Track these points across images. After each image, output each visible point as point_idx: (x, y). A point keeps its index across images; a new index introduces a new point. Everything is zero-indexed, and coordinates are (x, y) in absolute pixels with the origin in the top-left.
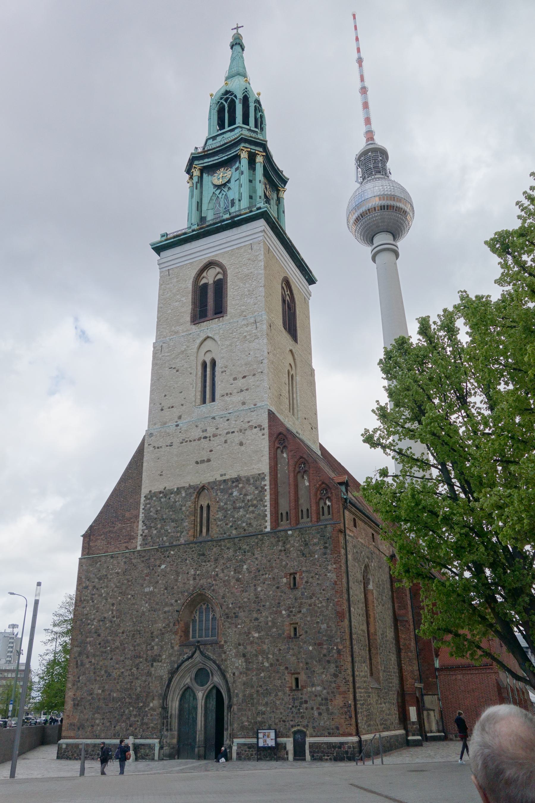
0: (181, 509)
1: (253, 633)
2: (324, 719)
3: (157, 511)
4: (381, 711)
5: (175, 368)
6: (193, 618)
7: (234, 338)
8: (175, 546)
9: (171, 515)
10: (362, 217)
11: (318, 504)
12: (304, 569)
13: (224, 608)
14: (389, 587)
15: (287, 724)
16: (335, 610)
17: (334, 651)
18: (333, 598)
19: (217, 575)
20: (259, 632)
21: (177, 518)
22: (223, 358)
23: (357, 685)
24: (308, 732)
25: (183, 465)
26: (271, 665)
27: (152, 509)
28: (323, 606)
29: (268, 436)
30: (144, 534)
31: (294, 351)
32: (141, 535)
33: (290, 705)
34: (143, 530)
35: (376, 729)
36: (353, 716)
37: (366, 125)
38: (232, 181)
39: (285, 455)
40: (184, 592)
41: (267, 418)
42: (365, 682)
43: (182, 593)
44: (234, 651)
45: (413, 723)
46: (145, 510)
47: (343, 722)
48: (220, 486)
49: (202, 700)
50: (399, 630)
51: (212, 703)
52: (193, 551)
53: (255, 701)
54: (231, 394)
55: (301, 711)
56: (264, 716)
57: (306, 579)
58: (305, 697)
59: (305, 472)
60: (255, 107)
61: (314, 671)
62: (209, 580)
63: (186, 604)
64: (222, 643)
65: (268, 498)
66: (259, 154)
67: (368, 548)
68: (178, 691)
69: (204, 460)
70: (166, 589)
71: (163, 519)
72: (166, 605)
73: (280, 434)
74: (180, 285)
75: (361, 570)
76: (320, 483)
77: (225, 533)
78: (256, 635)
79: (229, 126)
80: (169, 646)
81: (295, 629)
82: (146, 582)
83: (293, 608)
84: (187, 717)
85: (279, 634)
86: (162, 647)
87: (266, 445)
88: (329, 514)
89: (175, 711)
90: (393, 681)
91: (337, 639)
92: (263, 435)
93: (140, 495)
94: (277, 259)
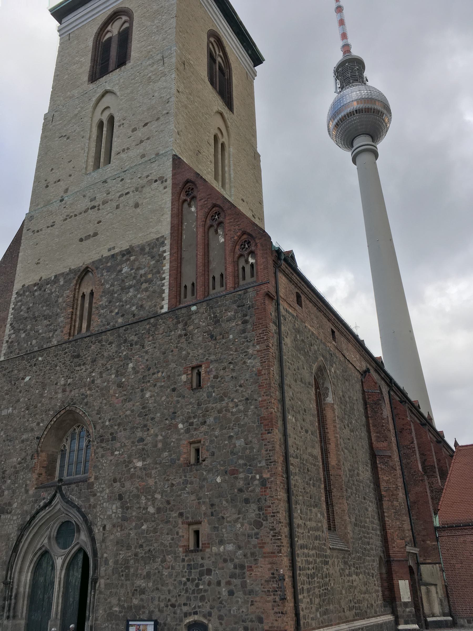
0: (57, 301)
1: (135, 461)
2: (237, 602)
3: (28, 308)
4: (351, 587)
5: (66, 136)
6: (62, 448)
7: (136, 83)
9: (45, 311)
10: (342, 122)
11: (236, 264)
12: (212, 357)
13: (98, 427)
14: (362, 410)
15: (178, 612)
16: (258, 415)
17: (256, 482)
18: (255, 396)
19: (93, 382)
20: (144, 460)
21: (50, 314)
23: (299, 542)
24: (210, 626)
26: (159, 510)
27: (23, 307)
28: (240, 411)
29: (171, 188)
30: (10, 341)
33: (183, 577)
34: (9, 335)
35: (340, 618)
36: (289, 596)
37: (343, 40)
39: (193, 209)
40: (49, 410)
41: (171, 166)
42: (316, 538)
43: (47, 411)
44: (107, 491)
45: (406, 604)
47: (271, 608)
48: (107, 263)
49: (61, 570)
50: (379, 469)
51: (76, 574)
52: (66, 353)
53: (132, 570)
54: (128, 149)
55: (201, 587)
56: (143, 596)
57: (214, 373)
58: (207, 563)
59: (220, 224)
61: (223, 518)
62: (83, 390)
63: (49, 426)
64: (92, 480)
65: (167, 267)
68: (30, 556)
69: (90, 235)
70: (27, 409)
71: (35, 318)
72: (26, 430)
73: (188, 182)
76: (239, 234)
77: (108, 324)
78: (140, 464)
80: (23, 490)
81: (197, 451)
82: (5, 402)
83: (194, 418)
84: (41, 597)
85: (172, 459)
86: (14, 492)
87: (168, 199)
88: (252, 276)
89: (25, 588)
90: (371, 541)
91: (260, 462)
92: (165, 188)
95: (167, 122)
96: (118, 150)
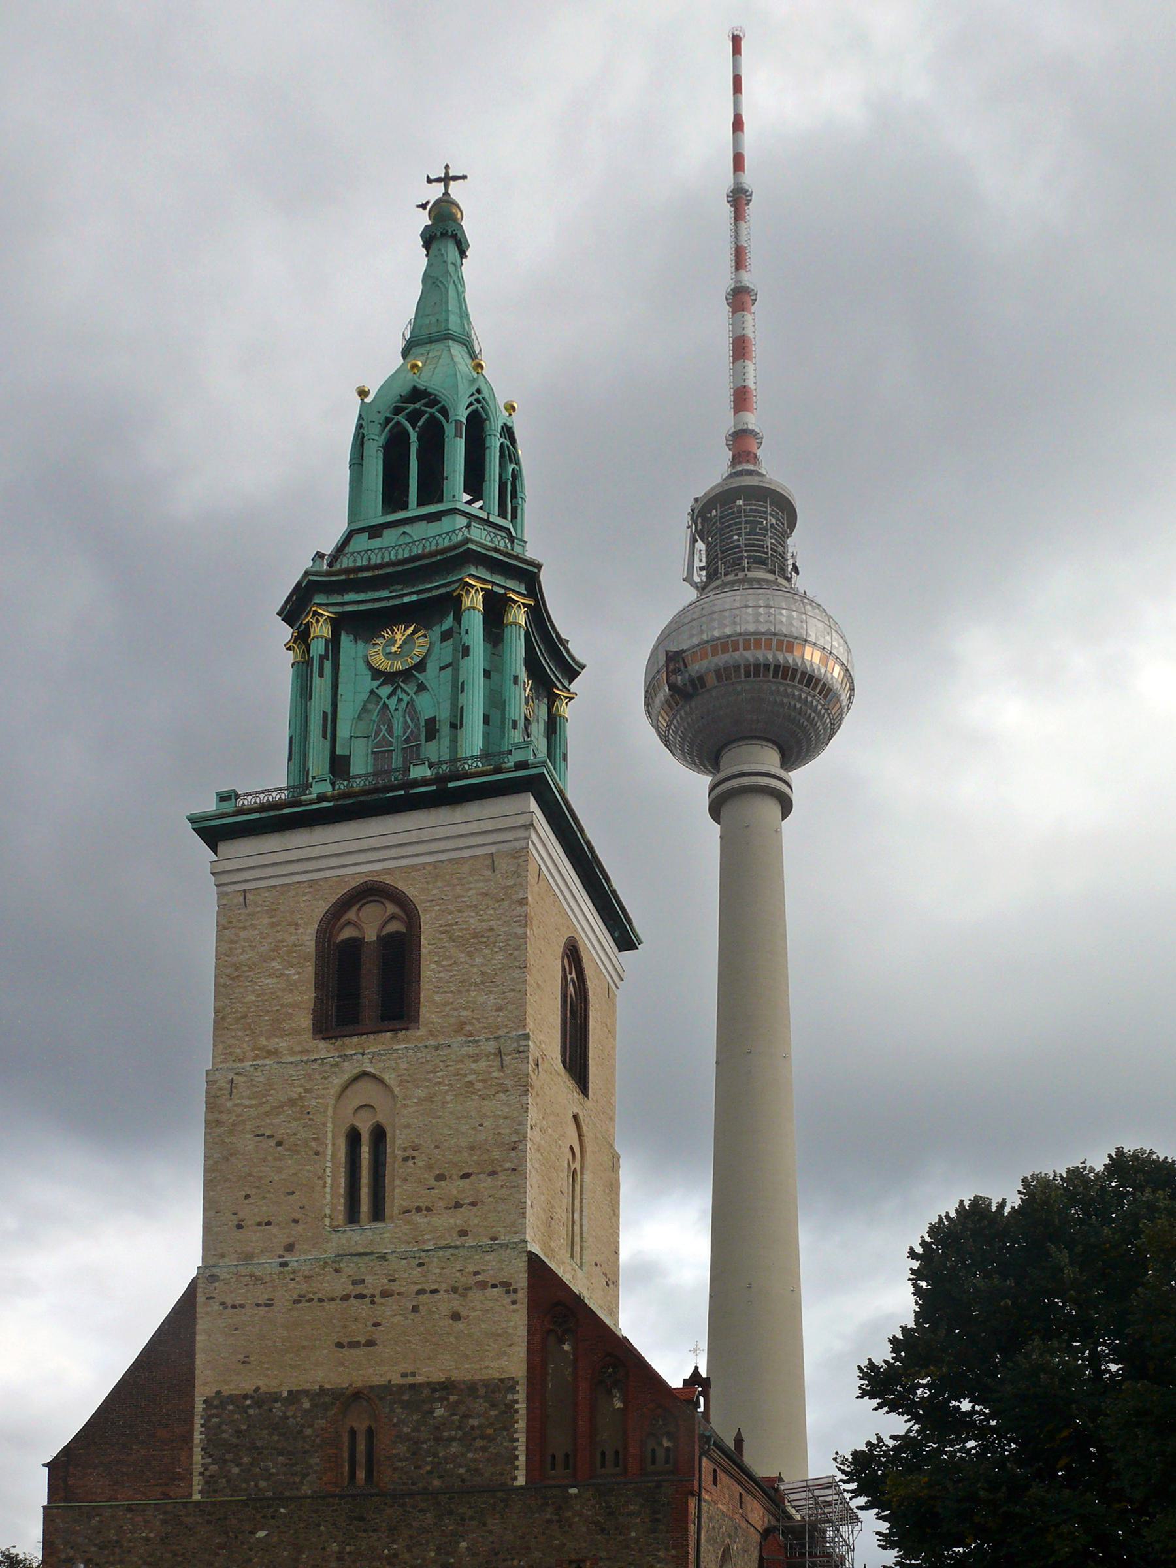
0: (300, 1432)
7: (439, 1083)
8: (288, 1498)
22: (408, 1126)
25: (304, 1348)
27: (224, 1427)
30: (207, 1473)
31: (581, 1116)
32: (201, 1474)
34: (203, 1465)
38: (432, 667)
46: (208, 1428)
54: (428, 1209)
60: (502, 444)
65: (521, 1425)
66: (515, 602)
67: (731, 1519)
71: (257, 1448)
74: (280, 936)
75: (717, 1557)
77: (413, 1484)
79: (420, 504)
92: (514, 1302)
93: (193, 1397)
94: (555, 894)
95: (515, 1187)
96: (404, 1204)
